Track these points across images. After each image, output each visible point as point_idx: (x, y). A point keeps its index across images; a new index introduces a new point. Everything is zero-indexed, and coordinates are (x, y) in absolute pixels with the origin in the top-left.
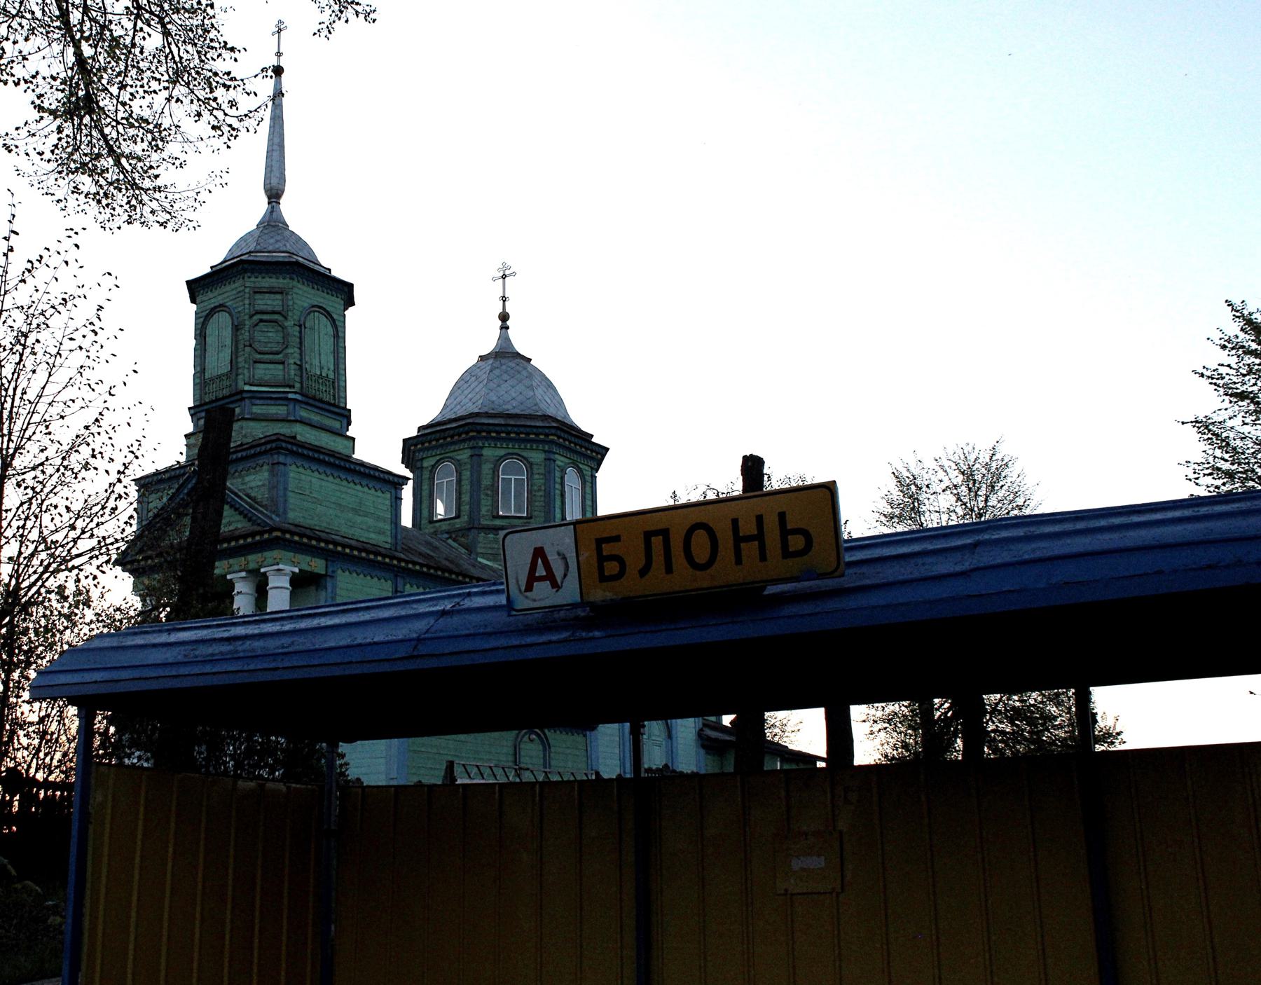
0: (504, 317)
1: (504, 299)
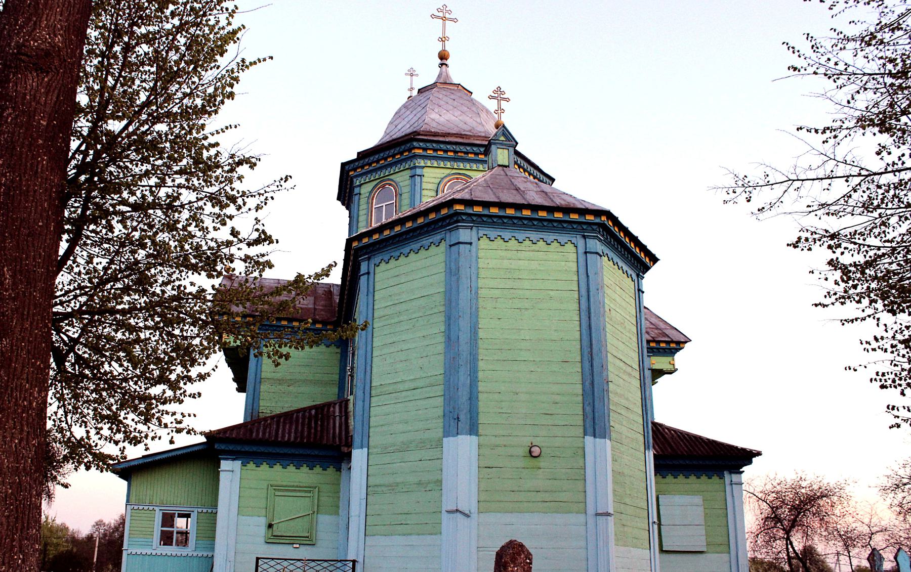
0: (443, 56)
1: (443, 40)
